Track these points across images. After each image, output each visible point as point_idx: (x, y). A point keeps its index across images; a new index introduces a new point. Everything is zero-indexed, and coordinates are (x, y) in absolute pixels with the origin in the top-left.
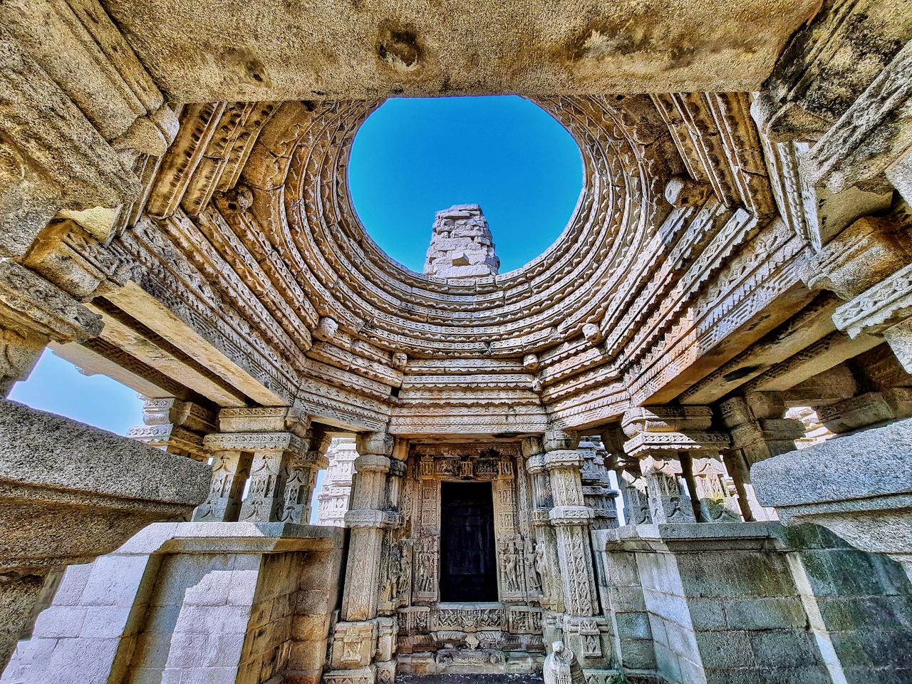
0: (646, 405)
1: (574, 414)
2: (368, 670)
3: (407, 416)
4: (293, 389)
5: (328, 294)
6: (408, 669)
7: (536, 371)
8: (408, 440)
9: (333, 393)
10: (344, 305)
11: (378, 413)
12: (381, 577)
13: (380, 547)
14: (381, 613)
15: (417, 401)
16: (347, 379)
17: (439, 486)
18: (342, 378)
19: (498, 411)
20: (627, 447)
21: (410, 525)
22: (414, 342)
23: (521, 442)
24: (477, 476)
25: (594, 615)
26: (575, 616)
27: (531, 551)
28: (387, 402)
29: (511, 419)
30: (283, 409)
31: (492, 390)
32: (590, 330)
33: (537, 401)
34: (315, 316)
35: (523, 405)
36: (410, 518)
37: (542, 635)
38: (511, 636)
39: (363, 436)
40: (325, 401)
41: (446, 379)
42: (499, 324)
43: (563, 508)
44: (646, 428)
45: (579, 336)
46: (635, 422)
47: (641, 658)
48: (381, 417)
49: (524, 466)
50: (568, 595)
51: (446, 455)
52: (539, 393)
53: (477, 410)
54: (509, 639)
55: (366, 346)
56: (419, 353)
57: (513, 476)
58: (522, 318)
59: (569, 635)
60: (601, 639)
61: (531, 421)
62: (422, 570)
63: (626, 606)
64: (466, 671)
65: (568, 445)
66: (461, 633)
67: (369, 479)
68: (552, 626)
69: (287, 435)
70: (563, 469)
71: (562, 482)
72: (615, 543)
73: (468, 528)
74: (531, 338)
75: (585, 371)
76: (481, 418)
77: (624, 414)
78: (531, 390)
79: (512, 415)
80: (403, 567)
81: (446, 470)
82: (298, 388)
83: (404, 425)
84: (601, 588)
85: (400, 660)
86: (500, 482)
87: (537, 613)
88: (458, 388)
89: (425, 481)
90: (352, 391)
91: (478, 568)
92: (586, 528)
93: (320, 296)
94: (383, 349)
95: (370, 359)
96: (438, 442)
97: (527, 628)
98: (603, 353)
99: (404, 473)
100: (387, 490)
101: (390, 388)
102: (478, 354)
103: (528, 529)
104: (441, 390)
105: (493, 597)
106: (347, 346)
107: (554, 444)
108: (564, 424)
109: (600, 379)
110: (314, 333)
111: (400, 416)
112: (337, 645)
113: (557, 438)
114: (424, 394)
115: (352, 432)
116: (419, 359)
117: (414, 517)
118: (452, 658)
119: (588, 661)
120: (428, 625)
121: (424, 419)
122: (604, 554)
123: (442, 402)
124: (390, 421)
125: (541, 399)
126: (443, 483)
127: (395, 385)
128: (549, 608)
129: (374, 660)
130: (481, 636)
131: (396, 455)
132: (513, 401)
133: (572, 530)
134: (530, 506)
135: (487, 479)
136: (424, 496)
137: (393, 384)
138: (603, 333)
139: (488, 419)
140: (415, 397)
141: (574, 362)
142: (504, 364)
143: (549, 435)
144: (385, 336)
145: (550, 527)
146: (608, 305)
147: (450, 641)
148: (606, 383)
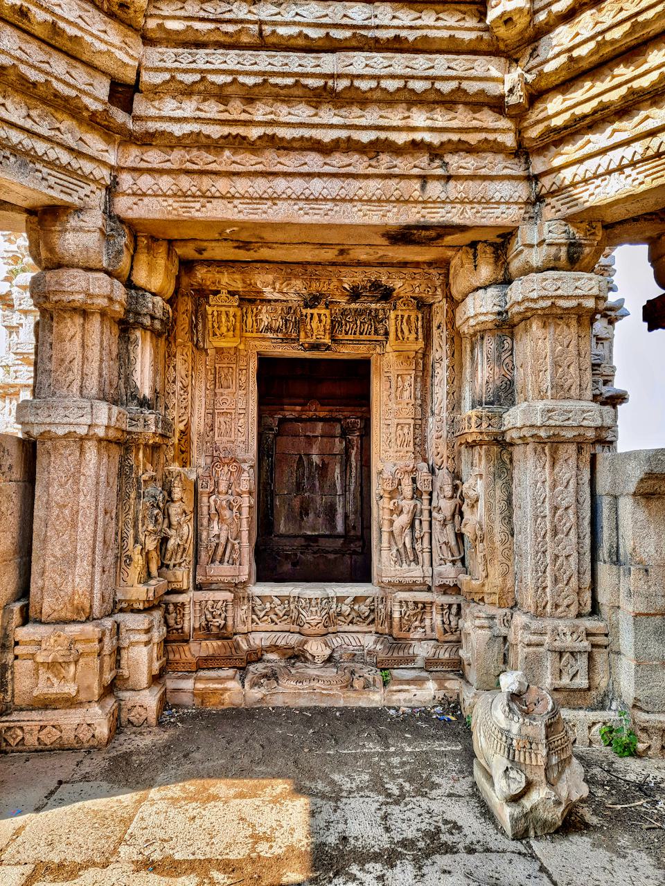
2: (96, 709)
3: (161, 172)
6: (186, 699)
8: (171, 243)
11: (79, 154)
13: (114, 481)
14: (124, 605)
15: (187, 128)
17: (253, 365)
19: (403, 165)
21: (189, 441)
26: (539, 614)
27: (449, 494)
28: (96, 123)
33: (509, 140)
36: (187, 426)
37: (459, 641)
38: (396, 643)
39: (45, 217)
41: (264, 61)
49: (451, 321)
50: (529, 578)
51: (269, 293)
53: (345, 160)
54: (391, 648)
57: (421, 344)
60: (591, 657)
61: (496, 199)
64: (303, 702)
66: (296, 636)
67: (72, 327)
71: (545, 347)
73: (316, 459)
79: (439, 178)
80: (174, 520)
84: (604, 569)
86: (391, 357)
87: (450, 606)
89: (219, 351)
91: (333, 526)
97: (428, 629)
104: (250, 97)
105: (362, 573)
107: (536, 257)
108: (573, 201)
114: (205, 106)
118: (277, 679)
119: (557, 695)
120: (230, 622)
122: (627, 506)
123: (254, 133)
124: (115, 183)
125: (519, 132)
128: (482, 600)
129: (110, 689)
130: (336, 641)
132: (445, 137)
133: (554, 452)
136: (217, 381)
139: (373, 187)
140: (178, 114)
143: (528, 234)
145: (501, 445)
147: (274, 648)
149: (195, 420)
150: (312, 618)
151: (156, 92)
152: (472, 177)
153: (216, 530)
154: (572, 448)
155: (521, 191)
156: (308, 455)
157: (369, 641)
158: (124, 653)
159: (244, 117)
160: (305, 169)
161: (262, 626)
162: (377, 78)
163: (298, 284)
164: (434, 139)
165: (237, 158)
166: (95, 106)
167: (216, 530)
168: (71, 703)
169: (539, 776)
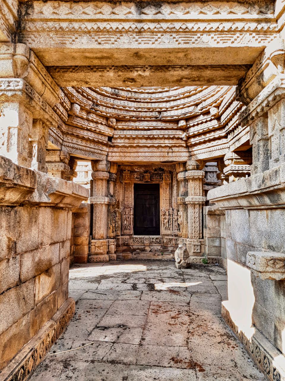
0: (235, 152)
1: (202, 152)
2: (106, 255)
3: (117, 152)
4: (61, 141)
5: (75, 91)
6: (121, 257)
7: (185, 129)
9: (80, 142)
10: (83, 95)
12: (108, 224)
16: (85, 134)
17: (133, 186)
18: (83, 134)
19: (163, 150)
20: (225, 170)
21: (119, 203)
22: (119, 112)
23: (175, 165)
24: (152, 181)
25: (199, 239)
28: (106, 145)
29: (170, 154)
30: (58, 151)
31: (161, 139)
32: (214, 111)
34: (69, 104)
35: (177, 147)
40: (76, 146)
41: (137, 133)
42: (167, 101)
43: (191, 197)
44: (233, 162)
45: (208, 113)
46: (229, 159)
47: (215, 252)
48: (103, 152)
49: (176, 177)
50: (190, 232)
51: (136, 170)
52: (186, 141)
53: (153, 149)
54: (164, 248)
55: (94, 116)
56: (122, 118)
57: (170, 181)
58: (179, 99)
59: (188, 245)
61: (181, 155)
62: (125, 222)
63: (213, 235)
65: (198, 168)
68: (182, 243)
69: (61, 164)
70: (194, 179)
72: (211, 211)
73: (147, 206)
74: (184, 111)
75: (209, 131)
76: (155, 153)
77: (225, 155)
78: (181, 139)
80: (117, 221)
81: (136, 178)
82: (63, 140)
83: (115, 157)
85: (118, 254)
86: (164, 184)
88: (143, 138)
89: (126, 183)
90: (88, 140)
91: (152, 224)
92: (201, 205)
93: (71, 94)
94: (103, 117)
95: (97, 123)
96: (132, 164)
98: (219, 123)
99: (116, 179)
100: (108, 188)
101: (107, 137)
102: (154, 119)
103: (176, 206)
104: (134, 139)
106: (85, 117)
107: (191, 167)
109: (217, 136)
110: (69, 113)
111: (113, 152)
112: (93, 247)
113: (193, 164)
114: (125, 140)
115: (89, 160)
116: (122, 121)
117: (121, 199)
121: (125, 154)
122: (207, 216)
123: (135, 145)
124: (108, 154)
125: (186, 144)
126: (135, 184)
127: (110, 136)
130: (152, 247)
131: (112, 171)
132: (172, 145)
133: (194, 206)
134: (178, 195)
135: (157, 182)
136: (125, 190)
137: (109, 135)
138: (220, 113)
139: (158, 154)
140: (120, 142)
141: (205, 127)
142: (168, 125)
143: (189, 163)
144: (104, 110)
146: (223, 100)
147: (138, 249)
148: (220, 138)
149: (120, 198)
150: (147, 242)
151: (116, 138)
152: (178, 152)
153: (125, 223)
154: (198, 206)
155: (187, 154)
156: (145, 204)
157: (159, 248)
158: (110, 247)
159: (133, 142)
160: (145, 151)
161: (136, 244)
162: (158, 135)
163: (143, 168)
164: (170, 145)
165: (131, 149)
166: (105, 142)
167: (125, 223)
168: (101, 254)
169: (182, 259)
